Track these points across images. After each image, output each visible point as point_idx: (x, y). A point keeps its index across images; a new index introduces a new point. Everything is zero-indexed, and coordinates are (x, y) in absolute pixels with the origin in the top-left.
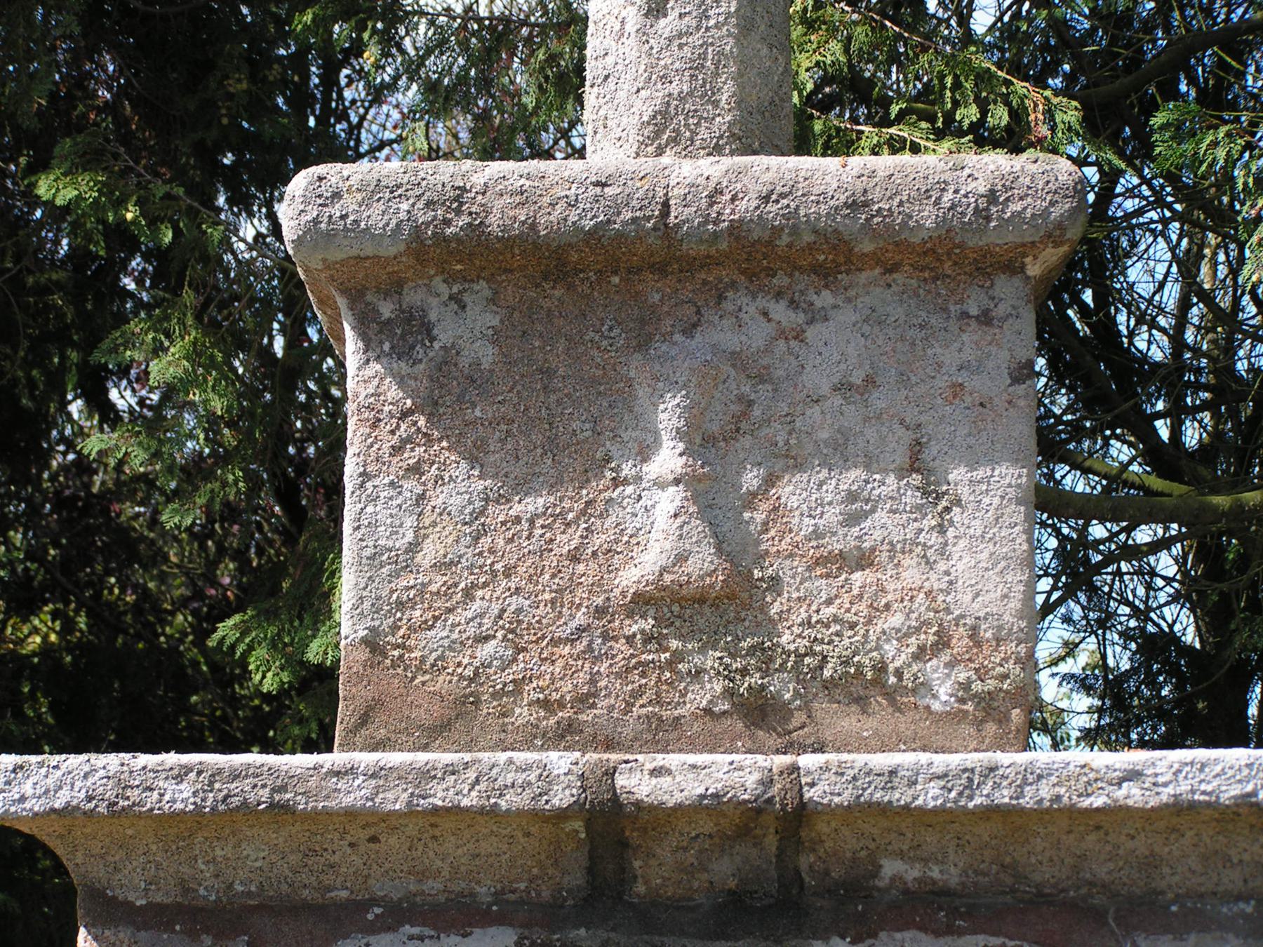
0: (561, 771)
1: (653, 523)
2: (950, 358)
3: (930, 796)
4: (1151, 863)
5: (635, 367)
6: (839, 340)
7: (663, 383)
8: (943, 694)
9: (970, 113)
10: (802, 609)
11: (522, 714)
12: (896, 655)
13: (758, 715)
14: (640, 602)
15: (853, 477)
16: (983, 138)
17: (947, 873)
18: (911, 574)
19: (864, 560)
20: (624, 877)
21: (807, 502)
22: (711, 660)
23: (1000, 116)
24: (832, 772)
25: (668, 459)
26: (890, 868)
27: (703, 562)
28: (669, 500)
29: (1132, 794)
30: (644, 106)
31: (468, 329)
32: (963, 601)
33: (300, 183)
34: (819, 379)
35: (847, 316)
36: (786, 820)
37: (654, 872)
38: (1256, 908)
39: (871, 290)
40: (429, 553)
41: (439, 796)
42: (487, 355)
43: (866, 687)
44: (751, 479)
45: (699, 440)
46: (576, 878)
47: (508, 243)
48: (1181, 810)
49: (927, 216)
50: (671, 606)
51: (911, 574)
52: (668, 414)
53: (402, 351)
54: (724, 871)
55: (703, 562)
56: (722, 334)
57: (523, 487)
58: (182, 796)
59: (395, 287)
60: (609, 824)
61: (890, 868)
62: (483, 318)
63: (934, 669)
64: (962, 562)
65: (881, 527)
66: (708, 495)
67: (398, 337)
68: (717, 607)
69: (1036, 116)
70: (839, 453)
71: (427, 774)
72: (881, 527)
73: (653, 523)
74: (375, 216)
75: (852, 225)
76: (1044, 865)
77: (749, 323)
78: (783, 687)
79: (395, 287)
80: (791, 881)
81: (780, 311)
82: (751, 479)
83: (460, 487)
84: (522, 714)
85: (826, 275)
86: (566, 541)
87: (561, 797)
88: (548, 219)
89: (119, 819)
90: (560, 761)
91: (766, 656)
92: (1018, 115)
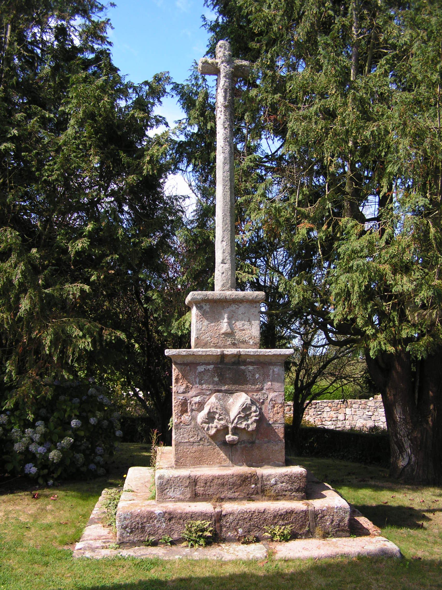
0: (218, 351)
1: (224, 326)
2: (252, 311)
3: (252, 354)
4: (271, 360)
5: (222, 311)
6: (242, 309)
7: (225, 313)
8: (251, 343)
9: (247, 270)
10: (238, 335)
11: (212, 344)
12: (247, 339)
13: (234, 345)
14: (223, 334)
15: (243, 322)
16: (248, 273)
17: (253, 360)
18: (248, 331)
19: (244, 330)
20: (224, 360)
21: (239, 324)
22: (230, 339)
23: (250, 270)
24: (243, 351)
25: (226, 320)
26: (248, 360)
27: (229, 330)
28: (226, 324)
29: (270, 353)
30: (222, 283)
31: (207, 307)
32: (253, 334)
33: (191, 293)
34: (240, 312)
35: (243, 307)
36: (239, 355)
37: (226, 360)
38: (7, 131)
39: (245, 305)
40: (203, 329)
41: (208, 353)
42: (208, 310)
43: (244, 342)
44: (233, 322)
45: (229, 318)
46: (219, 360)
47: (211, 300)
48: (274, 355)
49: (251, 298)
50: (226, 334)
51: (248, 331)
52: (226, 316)
53: (200, 309)
54: (233, 360)
55: (229, 330)
56: (231, 308)
57: (212, 323)
58: (184, 353)
59: (200, 303)
60: (223, 356)
61: (248, 360)
62: (208, 306)
63: (250, 340)
64: (253, 330)
65: (245, 327)
66: (229, 324)
67: (199, 308)
68: (230, 334)
69: (254, 271)
70: (242, 320)
71: (207, 351)
72: (245, 327)
73: (224, 326)
74: (198, 297)
75: (243, 298)
76: (262, 360)
77: (233, 307)
78: (236, 342)
79: (200, 303)
80: (239, 361)
81: (236, 306)
82: (233, 322)
83: (206, 323)
84: (212, 344)
85: (241, 303)
86: (216, 328)
87: (219, 354)
88: (215, 298)
89: (179, 356)
90: (219, 350)
91: (235, 339)
92: (252, 271)
